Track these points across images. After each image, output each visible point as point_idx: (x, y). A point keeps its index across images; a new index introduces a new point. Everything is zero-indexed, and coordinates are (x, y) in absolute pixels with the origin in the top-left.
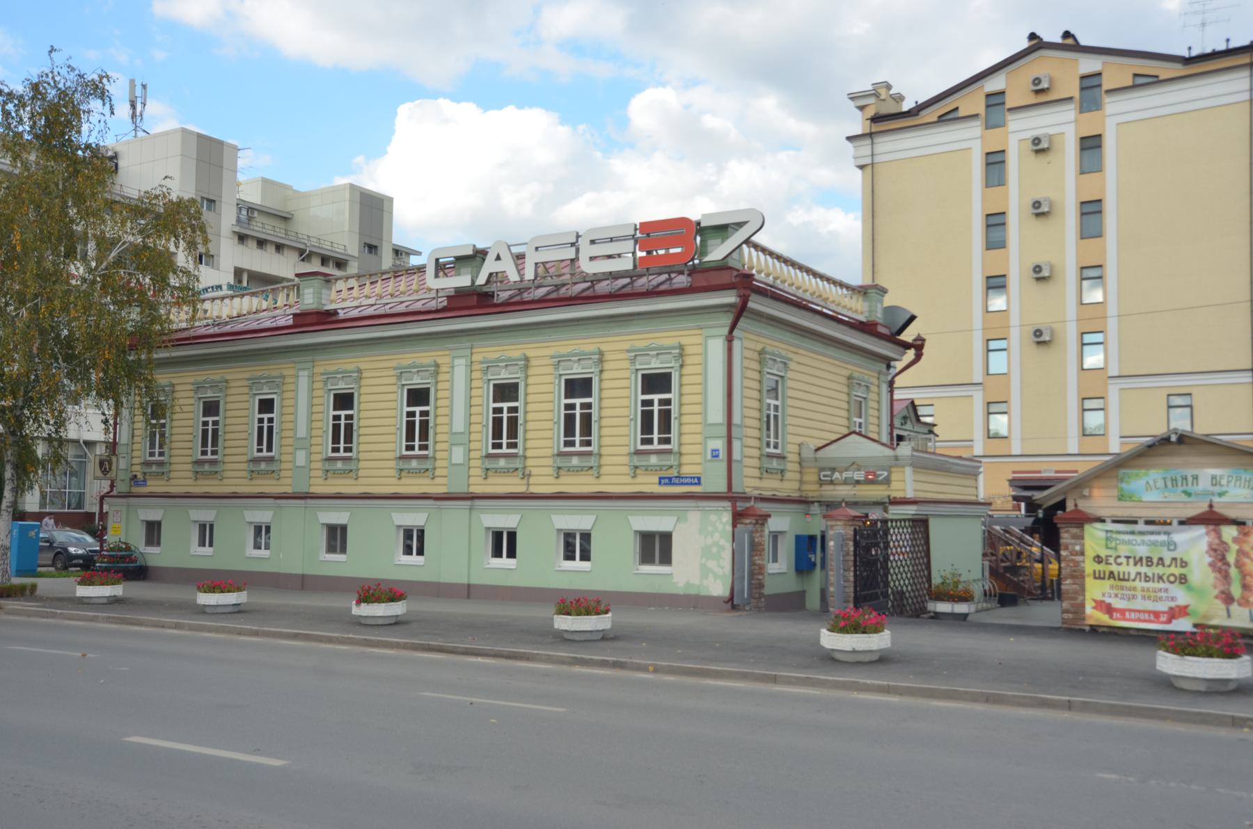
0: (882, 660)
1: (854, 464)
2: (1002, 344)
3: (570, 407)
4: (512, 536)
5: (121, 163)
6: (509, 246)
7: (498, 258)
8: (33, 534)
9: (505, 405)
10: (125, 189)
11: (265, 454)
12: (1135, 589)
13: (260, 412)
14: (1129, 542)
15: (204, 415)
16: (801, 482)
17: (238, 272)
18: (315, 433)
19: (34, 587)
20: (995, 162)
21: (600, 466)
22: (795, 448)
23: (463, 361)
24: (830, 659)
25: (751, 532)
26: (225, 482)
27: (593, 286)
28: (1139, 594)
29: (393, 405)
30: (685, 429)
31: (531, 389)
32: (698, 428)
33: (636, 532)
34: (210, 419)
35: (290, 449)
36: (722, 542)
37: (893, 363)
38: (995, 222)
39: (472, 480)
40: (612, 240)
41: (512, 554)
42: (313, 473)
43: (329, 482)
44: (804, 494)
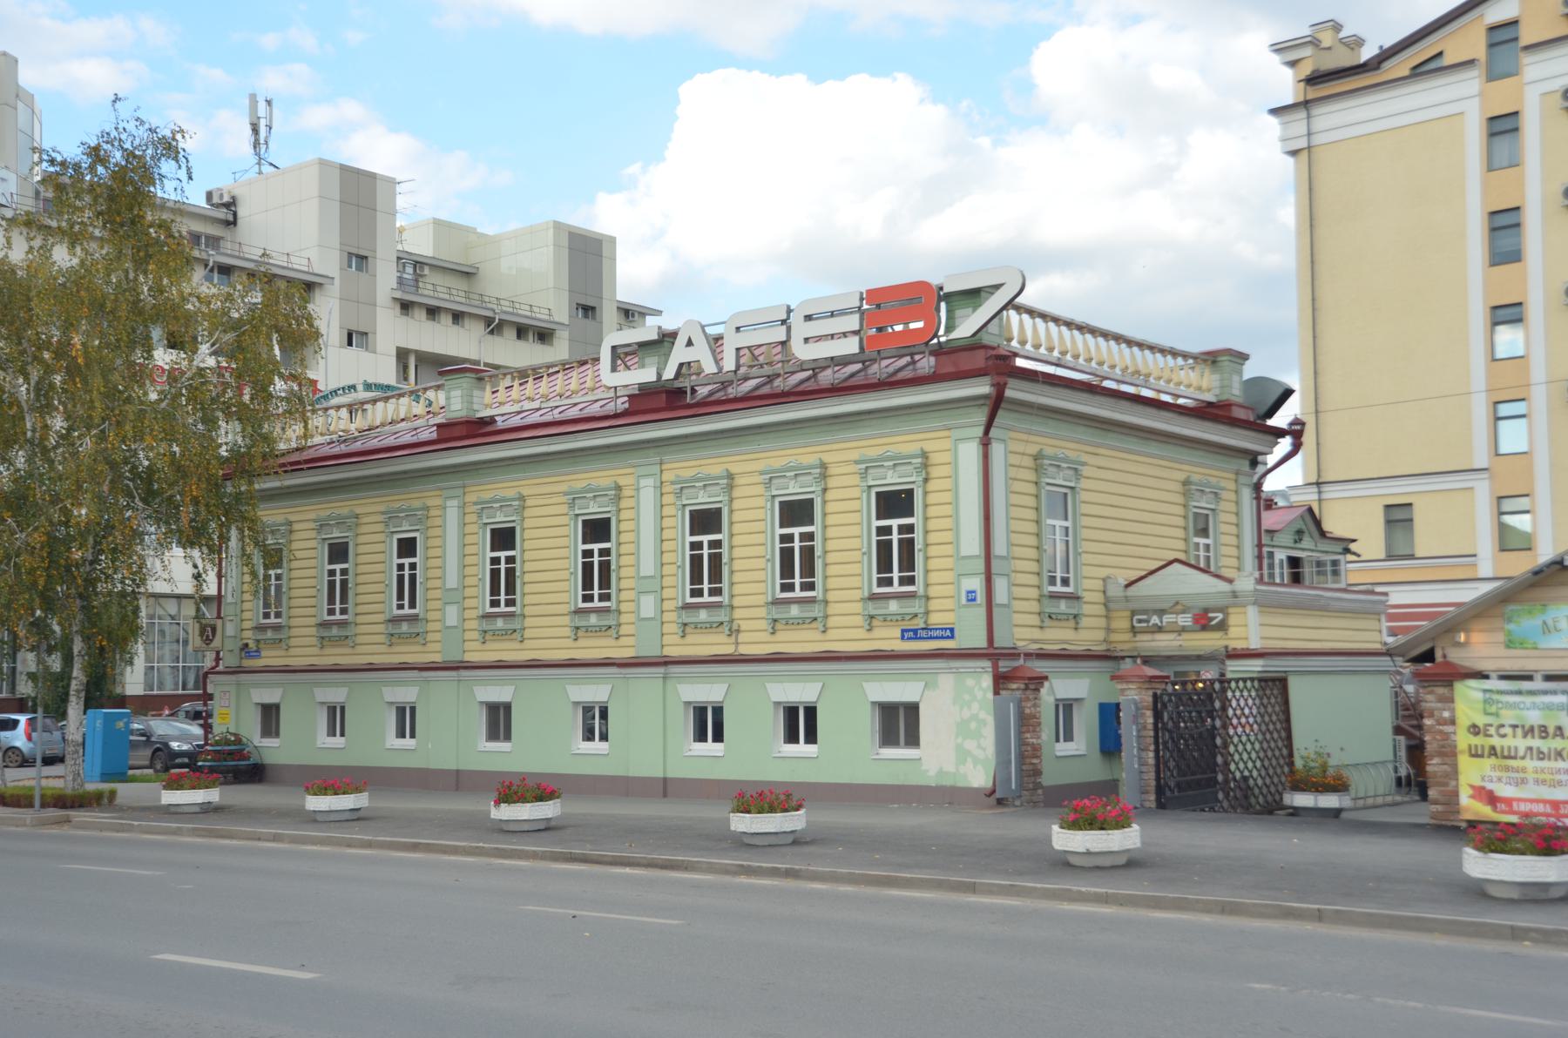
0: (1132, 863)
1: (1178, 606)
2: (1519, 408)
3: (787, 538)
4: (811, 712)
5: (241, 212)
6: (703, 327)
7: (690, 343)
8: (121, 724)
9: (705, 539)
10: (245, 249)
11: (407, 611)
12: (1524, 770)
13: (399, 557)
14: (1514, 706)
15: (330, 563)
16: (1109, 630)
17: (402, 355)
18: (469, 581)
19: (113, 794)
20: (1503, 126)
21: (826, 617)
22: (1099, 584)
23: (650, 482)
24: (1064, 864)
25: (1021, 701)
26: (359, 649)
27: (815, 375)
28: (1531, 776)
29: (564, 542)
30: (933, 564)
31: (737, 517)
32: (948, 563)
33: (873, 703)
35: (437, 604)
36: (983, 715)
37: (1260, 458)
38: (1504, 226)
39: (666, 639)
40: (832, 314)
41: (811, 737)
42: (468, 635)
43: (489, 645)
44: (1111, 647)
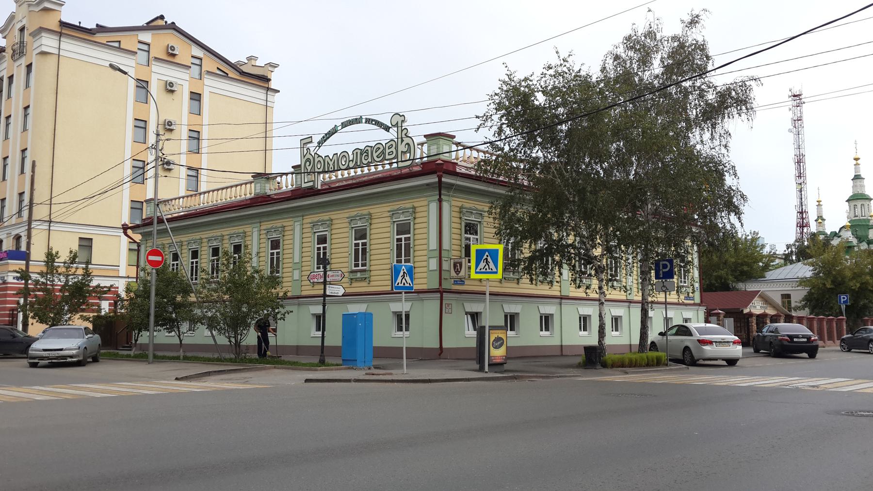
3: (399, 240)
32: (425, 253)
34: (275, 251)
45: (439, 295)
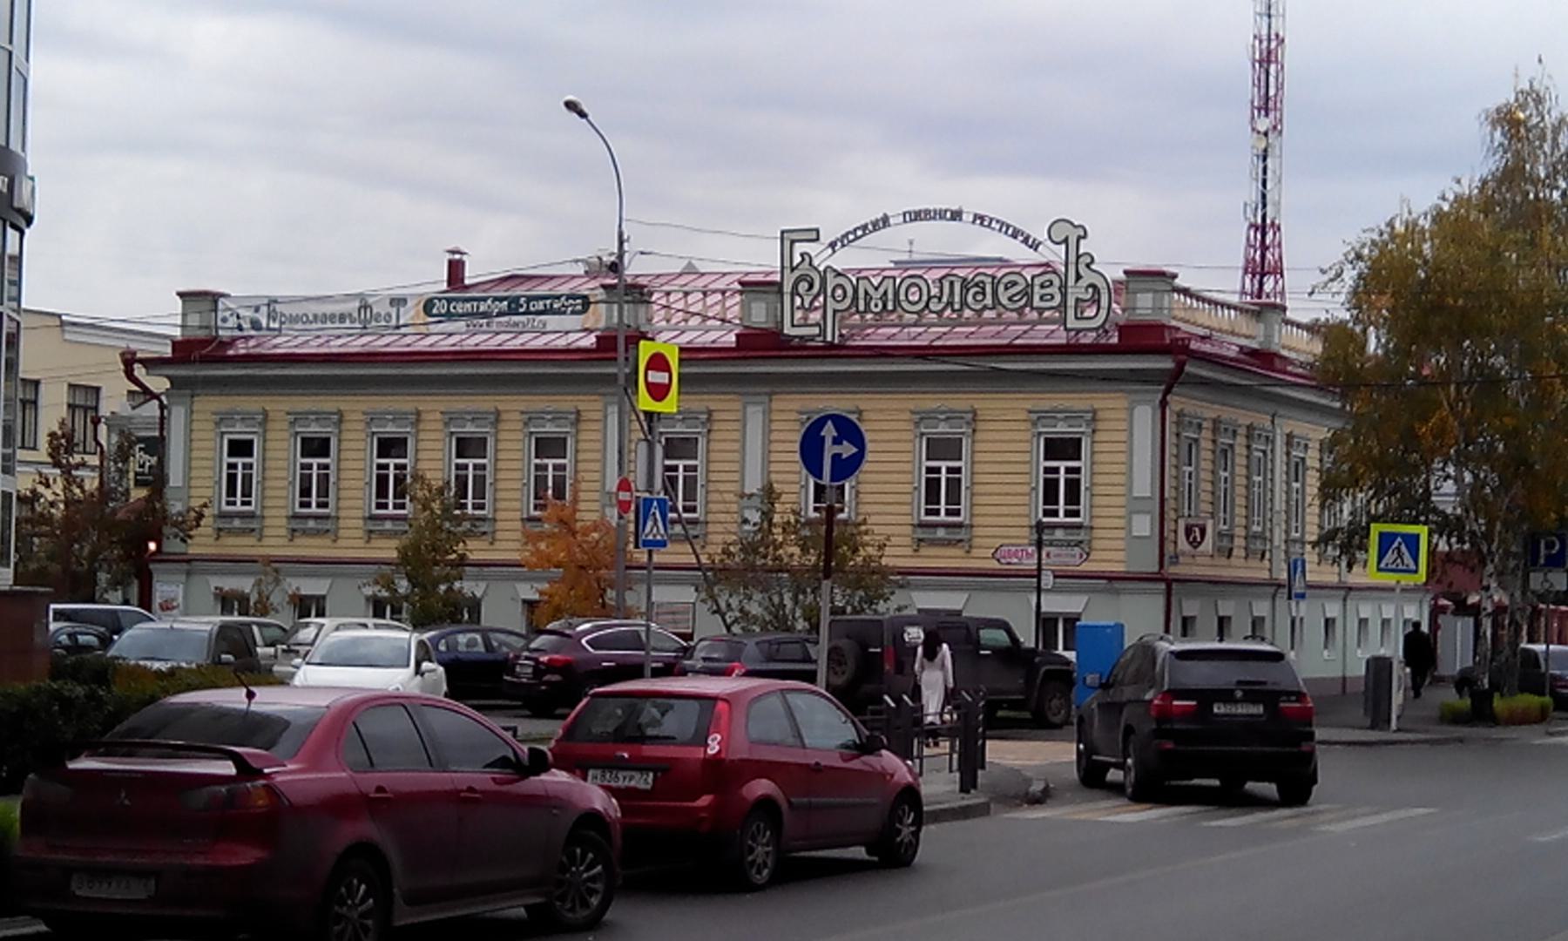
21: (706, 535)
45: (1163, 586)
